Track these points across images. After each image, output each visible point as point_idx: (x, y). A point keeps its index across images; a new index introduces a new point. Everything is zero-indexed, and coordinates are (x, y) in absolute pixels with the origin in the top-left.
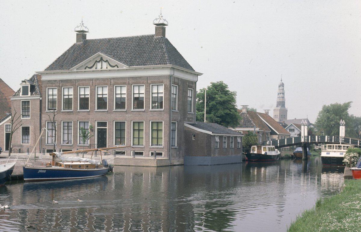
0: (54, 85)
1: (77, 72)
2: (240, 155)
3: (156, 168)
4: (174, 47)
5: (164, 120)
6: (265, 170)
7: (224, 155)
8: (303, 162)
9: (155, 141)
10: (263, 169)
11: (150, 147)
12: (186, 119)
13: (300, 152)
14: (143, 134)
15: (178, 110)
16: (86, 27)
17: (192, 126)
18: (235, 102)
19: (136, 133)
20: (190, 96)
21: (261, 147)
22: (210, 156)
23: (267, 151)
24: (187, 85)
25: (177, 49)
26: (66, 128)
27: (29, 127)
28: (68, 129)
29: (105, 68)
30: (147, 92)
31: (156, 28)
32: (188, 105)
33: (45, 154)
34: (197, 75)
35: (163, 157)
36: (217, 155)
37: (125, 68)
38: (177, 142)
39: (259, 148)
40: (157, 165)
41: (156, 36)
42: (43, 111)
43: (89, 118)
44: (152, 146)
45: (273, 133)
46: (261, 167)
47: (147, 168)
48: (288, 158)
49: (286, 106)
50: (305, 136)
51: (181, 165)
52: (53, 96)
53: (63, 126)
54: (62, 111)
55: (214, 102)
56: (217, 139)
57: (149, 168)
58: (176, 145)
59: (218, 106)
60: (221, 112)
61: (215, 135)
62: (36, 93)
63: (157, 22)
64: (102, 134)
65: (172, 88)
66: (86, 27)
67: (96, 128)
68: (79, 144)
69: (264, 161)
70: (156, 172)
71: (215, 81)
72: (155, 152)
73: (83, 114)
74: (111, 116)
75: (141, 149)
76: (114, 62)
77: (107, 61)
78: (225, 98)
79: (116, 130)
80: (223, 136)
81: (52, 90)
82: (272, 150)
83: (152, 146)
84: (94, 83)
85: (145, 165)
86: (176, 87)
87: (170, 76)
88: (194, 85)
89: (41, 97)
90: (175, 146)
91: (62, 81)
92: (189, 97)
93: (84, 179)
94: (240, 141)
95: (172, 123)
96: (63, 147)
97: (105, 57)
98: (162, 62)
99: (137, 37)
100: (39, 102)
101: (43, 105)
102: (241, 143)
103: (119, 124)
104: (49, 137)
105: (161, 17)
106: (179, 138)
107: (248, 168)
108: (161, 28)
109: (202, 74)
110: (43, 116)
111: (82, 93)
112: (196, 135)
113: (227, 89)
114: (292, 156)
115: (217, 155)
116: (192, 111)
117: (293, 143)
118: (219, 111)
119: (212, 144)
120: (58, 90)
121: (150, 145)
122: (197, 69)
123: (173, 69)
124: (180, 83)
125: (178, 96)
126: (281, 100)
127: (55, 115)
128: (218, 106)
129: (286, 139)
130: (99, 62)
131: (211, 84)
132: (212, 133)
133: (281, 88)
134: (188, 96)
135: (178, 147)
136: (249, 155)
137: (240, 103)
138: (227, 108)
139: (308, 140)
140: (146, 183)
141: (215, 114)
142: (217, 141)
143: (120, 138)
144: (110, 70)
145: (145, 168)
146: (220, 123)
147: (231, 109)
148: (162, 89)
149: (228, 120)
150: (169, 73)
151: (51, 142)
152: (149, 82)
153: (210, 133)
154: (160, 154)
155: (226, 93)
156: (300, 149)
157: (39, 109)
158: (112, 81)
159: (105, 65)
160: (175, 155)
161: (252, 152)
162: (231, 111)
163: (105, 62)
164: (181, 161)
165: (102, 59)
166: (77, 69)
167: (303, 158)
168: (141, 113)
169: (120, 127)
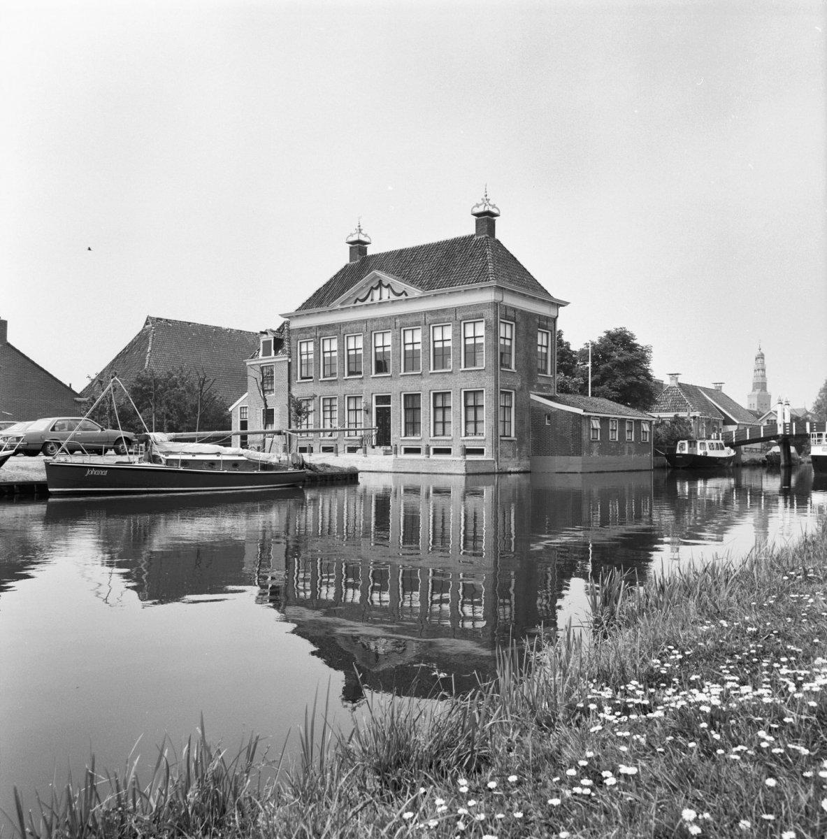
0: (308, 336)
1: (342, 309)
2: (647, 459)
4: (512, 256)
5: (487, 384)
6: (705, 483)
7: (612, 454)
8: (783, 471)
9: (471, 427)
10: (700, 484)
12: (535, 386)
13: (776, 455)
14: (450, 415)
16: (366, 236)
18: (647, 362)
19: (440, 413)
20: (545, 344)
21: (695, 442)
22: (580, 455)
23: (708, 450)
24: (535, 322)
25: (518, 259)
26: (328, 408)
28: (331, 411)
29: (390, 301)
30: (456, 335)
31: (477, 222)
32: (540, 361)
34: (558, 304)
35: (487, 456)
36: (595, 454)
37: (416, 295)
39: (693, 444)
40: (466, 471)
42: (293, 382)
43: (362, 391)
44: (466, 436)
45: (728, 421)
46: (697, 480)
47: (449, 477)
48: (754, 465)
49: (769, 389)
50: (785, 424)
51: (524, 472)
52: (308, 354)
53: (324, 406)
55: (608, 365)
56: (596, 424)
57: (452, 477)
58: (513, 435)
60: (621, 381)
61: (589, 417)
62: (284, 352)
64: (383, 417)
65: (502, 326)
67: (374, 406)
69: (704, 468)
70: (463, 484)
71: (612, 330)
73: (352, 386)
74: (396, 386)
75: (447, 443)
76: (400, 285)
77: (388, 286)
78: (629, 356)
79: (406, 409)
82: (721, 447)
83: (466, 436)
84: (370, 328)
85: (445, 471)
86: (512, 325)
87: (496, 304)
88: (550, 325)
89: (290, 357)
91: (320, 327)
92: (542, 346)
93: (200, 493)
94: (648, 430)
95: (502, 392)
96: (322, 442)
97: (387, 278)
98: (482, 276)
99: (446, 242)
100: (287, 367)
101: (293, 371)
102: (650, 433)
103: (410, 399)
105: (486, 202)
106: (520, 422)
107: (672, 481)
108: (486, 220)
109: (568, 303)
111: (351, 346)
112: (551, 415)
113: (635, 342)
114: (764, 461)
115: (595, 454)
116: (549, 372)
117: (762, 436)
119: (585, 434)
120: (315, 343)
122: (556, 294)
123: (499, 289)
125: (516, 342)
126: (760, 380)
129: (748, 430)
130: (376, 288)
131: (605, 334)
132: (584, 411)
133: (759, 361)
134: (539, 343)
135: (516, 439)
136: (671, 456)
137: (659, 369)
138: (634, 375)
139: (791, 430)
140: (456, 510)
141: (610, 385)
142: (595, 427)
143: (412, 426)
144: (393, 301)
145: (444, 476)
146: (618, 400)
147: (640, 375)
148: (481, 329)
152: (459, 317)
153: (580, 411)
154: (481, 452)
156: (777, 449)
157: (287, 378)
158: (398, 321)
159: (386, 292)
160: (510, 453)
161: (678, 452)
162: (639, 379)
163: (386, 287)
164: (525, 464)
165: (380, 284)
166: (342, 304)
167: (782, 463)
168: (447, 376)
169: (412, 402)
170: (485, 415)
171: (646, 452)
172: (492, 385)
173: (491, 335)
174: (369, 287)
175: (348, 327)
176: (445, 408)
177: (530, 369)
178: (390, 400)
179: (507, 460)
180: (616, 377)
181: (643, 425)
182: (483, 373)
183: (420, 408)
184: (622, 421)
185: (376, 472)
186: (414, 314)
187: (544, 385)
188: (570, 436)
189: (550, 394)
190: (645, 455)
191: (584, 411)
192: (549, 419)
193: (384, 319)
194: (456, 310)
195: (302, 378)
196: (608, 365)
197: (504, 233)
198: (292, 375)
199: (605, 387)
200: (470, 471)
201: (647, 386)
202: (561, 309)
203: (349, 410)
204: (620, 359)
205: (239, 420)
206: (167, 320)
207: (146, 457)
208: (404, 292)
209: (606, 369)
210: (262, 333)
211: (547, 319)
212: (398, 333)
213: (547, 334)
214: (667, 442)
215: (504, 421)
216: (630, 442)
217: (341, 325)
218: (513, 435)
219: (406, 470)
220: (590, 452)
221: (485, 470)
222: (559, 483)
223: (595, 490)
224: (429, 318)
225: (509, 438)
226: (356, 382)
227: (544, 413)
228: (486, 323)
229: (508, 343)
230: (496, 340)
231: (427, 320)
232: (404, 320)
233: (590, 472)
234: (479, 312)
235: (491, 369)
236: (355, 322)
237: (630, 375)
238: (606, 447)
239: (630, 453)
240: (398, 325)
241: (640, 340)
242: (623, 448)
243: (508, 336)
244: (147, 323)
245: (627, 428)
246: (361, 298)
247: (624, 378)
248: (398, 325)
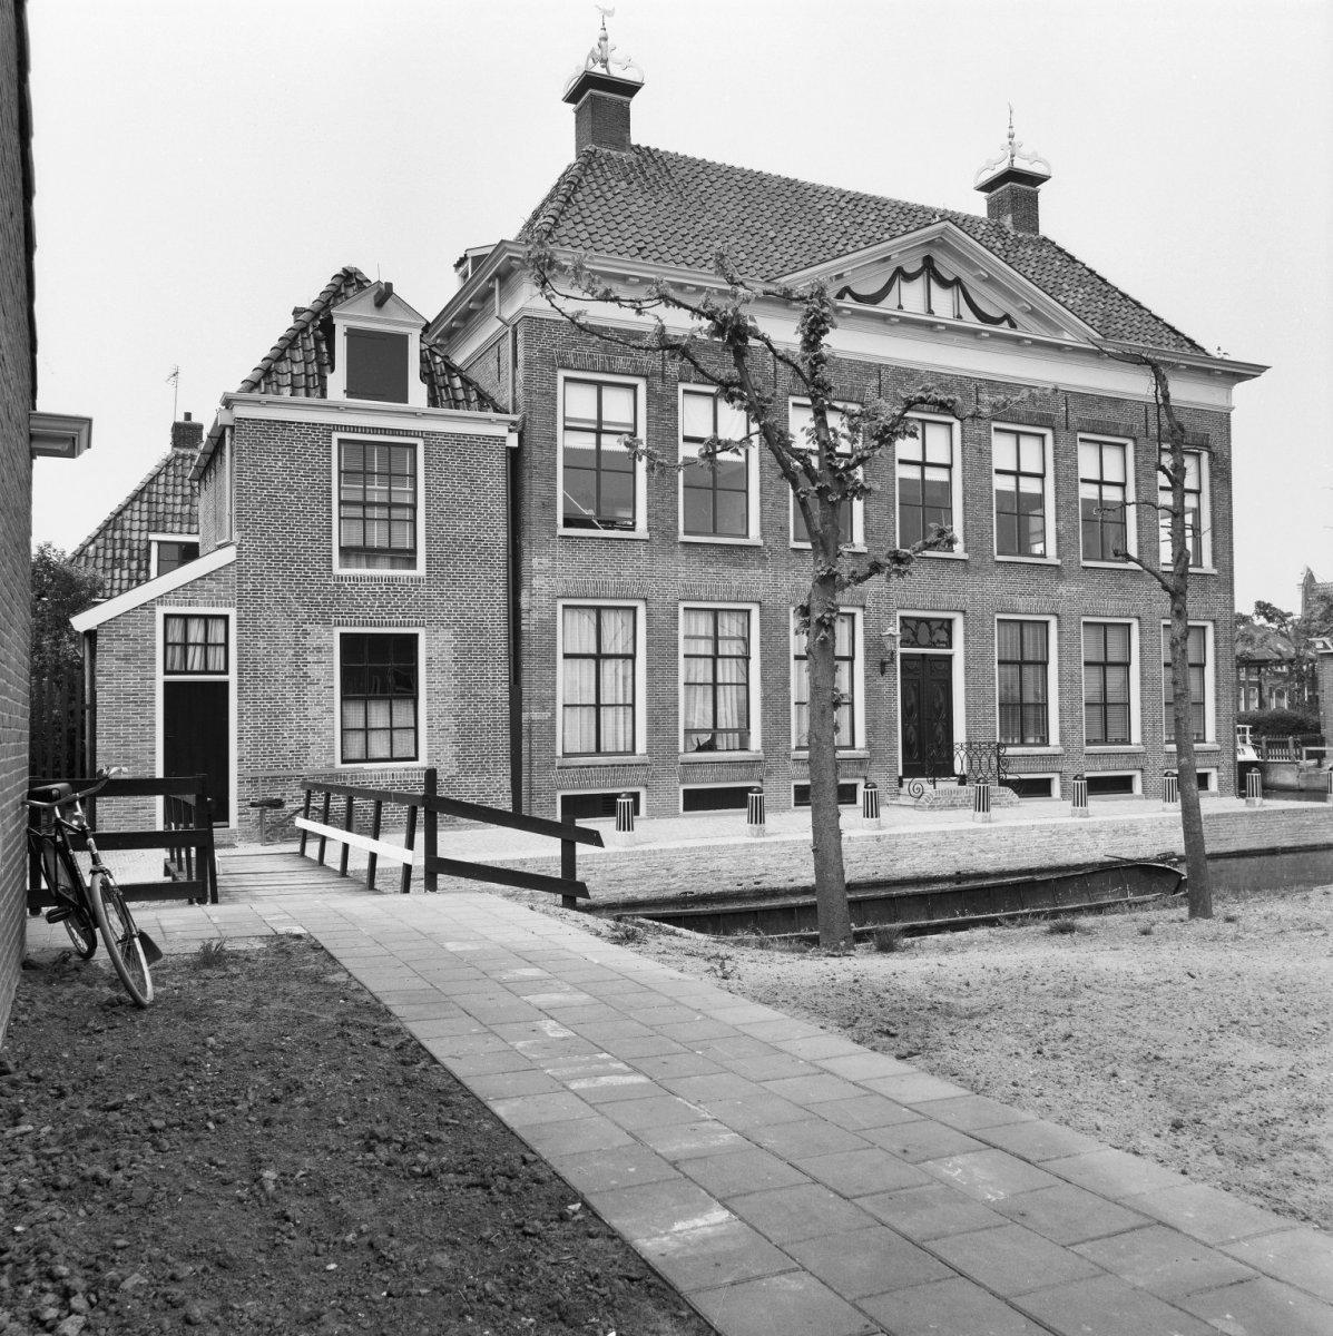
11: (680, 759)
27: (416, 636)
34: (1237, 373)
52: (599, 432)
54: (682, 538)
66: (1035, 154)
81: (591, 392)
100: (499, 464)
101: (533, 487)
108: (601, 99)
110: (535, 562)
122: (1217, 340)
168: (1126, 581)
202: (1240, 389)
229: (1112, 494)
243: (1113, 474)
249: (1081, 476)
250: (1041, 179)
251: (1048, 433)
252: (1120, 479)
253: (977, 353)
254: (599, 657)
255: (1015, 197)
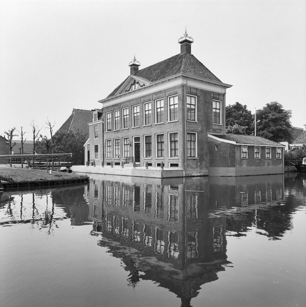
3: (161, 180)
5: (179, 129)
7: (256, 166)
14: (164, 147)
15: (198, 120)
16: (138, 62)
17: (216, 137)
24: (211, 96)
30: (166, 104)
33: (113, 166)
34: (226, 86)
35: (179, 168)
36: (245, 166)
38: (198, 152)
40: (162, 176)
41: (181, 54)
43: (129, 135)
51: (203, 176)
53: (115, 143)
55: (267, 120)
56: (245, 150)
57: (156, 179)
58: (196, 156)
59: (271, 124)
60: (273, 128)
63: (181, 40)
66: (138, 61)
67: (134, 142)
68: (108, 158)
72: (163, 162)
74: (142, 133)
77: (138, 83)
78: (278, 115)
79: (146, 143)
80: (254, 146)
85: (152, 176)
87: (183, 86)
90: (195, 157)
94: (281, 152)
95: (188, 133)
104: (108, 153)
106: (200, 149)
108: (186, 44)
112: (218, 145)
113: (283, 109)
115: (245, 166)
116: (221, 122)
118: (271, 128)
120: (112, 113)
121: (169, 156)
124: (199, 93)
125: (198, 106)
127: (51, 128)
128: (271, 124)
131: (266, 106)
132: (237, 143)
142: (278, 152)
143: (149, 152)
146: (270, 139)
147: (283, 125)
149: (281, 134)
150: (181, 83)
151: (109, 157)
153: (234, 143)
154: (177, 165)
155: (281, 111)
158: (142, 99)
160: (195, 166)
164: (204, 171)
166: (120, 93)
168: (162, 126)
170: (179, 146)
171: (280, 164)
172: (182, 129)
173: (181, 102)
174: (130, 84)
175: (123, 105)
176: (162, 142)
177: (207, 120)
178: (139, 139)
179: (192, 169)
180: (270, 126)
181: (278, 150)
182: (177, 123)
183: (151, 143)
184: (263, 148)
185: (125, 176)
186: (148, 95)
187: (217, 129)
188: (230, 156)
189: (221, 134)
190: (279, 166)
191: (237, 143)
192: (217, 147)
193: (136, 99)
194: (165, 91)
195: (108, 130)
196: (267, 120)
197: (196, 51)
198: (104, 129)
199: (265, 131)
200: (165, 176)
201: (287, 130)
202: (228, 90)
203: (124, 145)
204: (272, 117)
205: (87, 150)
206: (82, 110)
207: (54, 167)
208: (144, 84)
209: (265, 122)
210: (92, 110)
211: (219, 94)
212: (142, 106)
213: (220, 102)
214: (297, 158)
215: (191, 149)
216: (268, 159)
217: (121, 104)
218: (196, 156)
219: (137, 175)
220: (241, 164)
221: (176, 176)
222: (222, 182)
223: (245, 186)
224: (155, 97)
225: (269, 158)
226: (126, 131)
227: (214, 144)
228: (179, 96)
229: (218, 111)
230: (183, 105)
231: (154, 98)
232: (144, 99)
233: (241, 176)
234: (175, 91)
235: (181, 121)
236: (125, 102)
237: (278, 125)
238: (251, 161)
239: (269, 165)
240: (142, 102)
241: (285, 108)
242: (264, 162)
243: (218, 107)
244: (73, 112)
245: (255, 151)
246: (127, 90)
247: (275, 126)
248: (142, 102)
249: (213, 107)
250: (191, 42)
251: (196, 97)
252: (194, 104)
253: (210, 86)
254: (191, 141)
255: (186, 45)
